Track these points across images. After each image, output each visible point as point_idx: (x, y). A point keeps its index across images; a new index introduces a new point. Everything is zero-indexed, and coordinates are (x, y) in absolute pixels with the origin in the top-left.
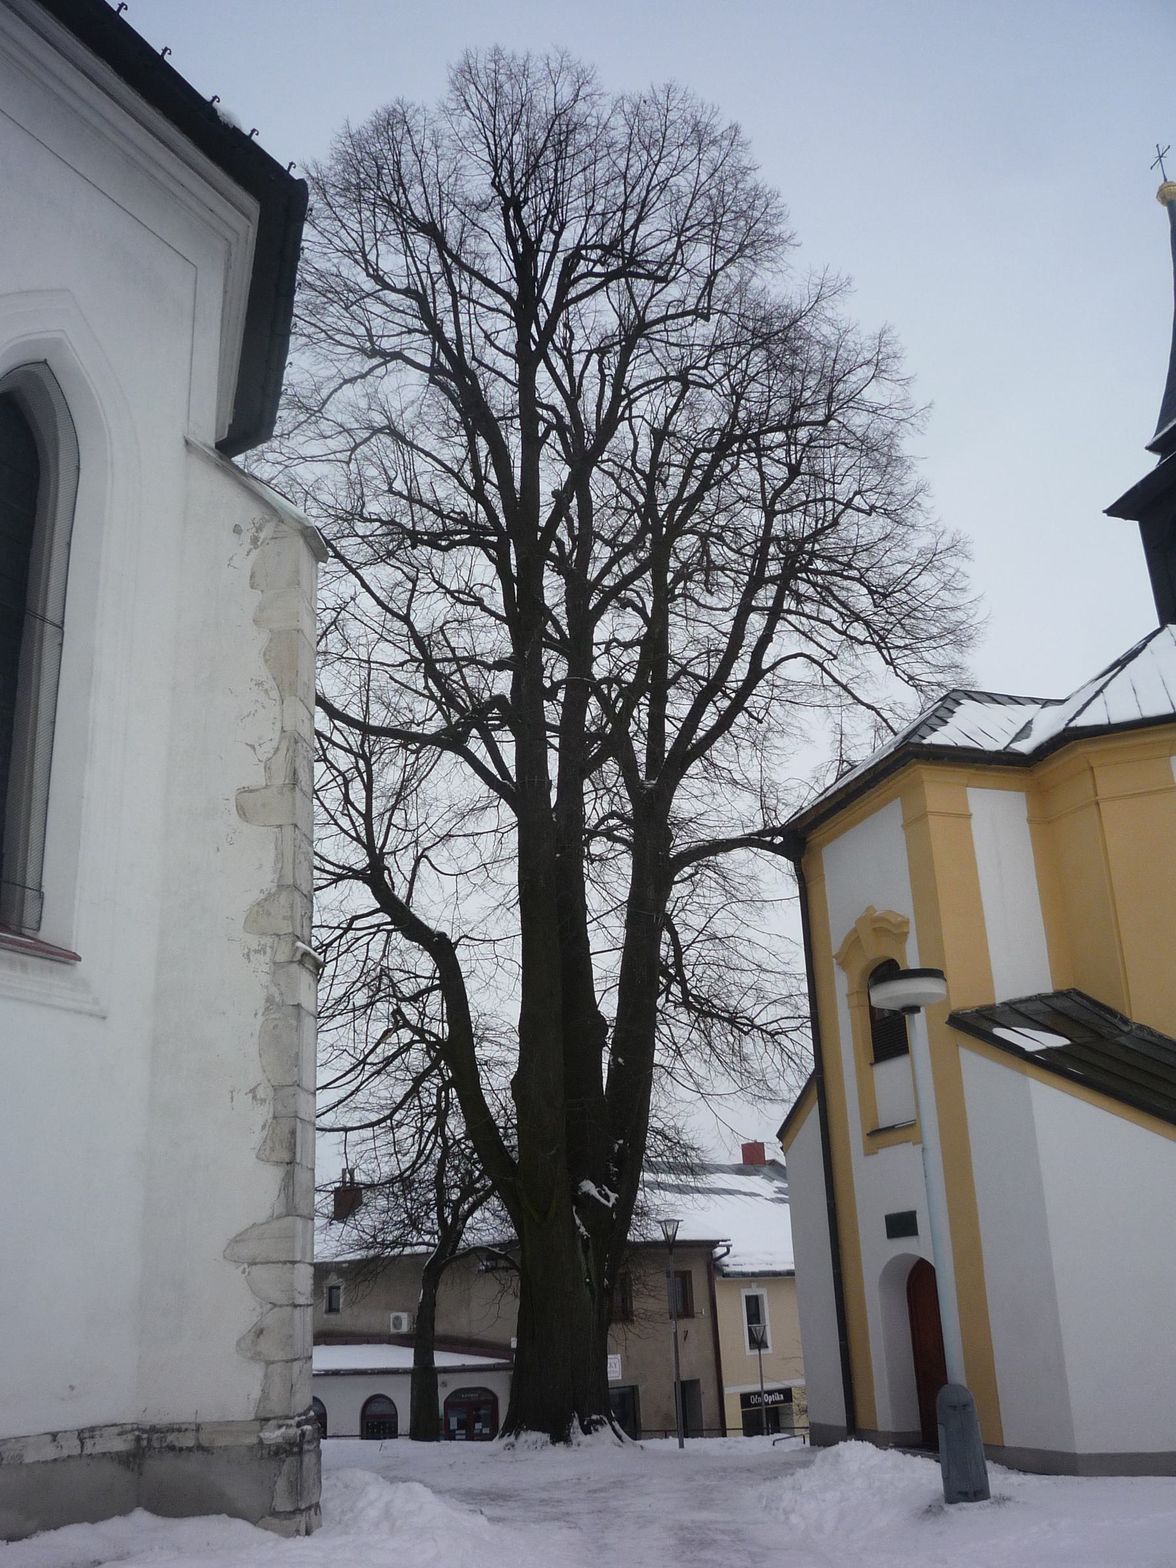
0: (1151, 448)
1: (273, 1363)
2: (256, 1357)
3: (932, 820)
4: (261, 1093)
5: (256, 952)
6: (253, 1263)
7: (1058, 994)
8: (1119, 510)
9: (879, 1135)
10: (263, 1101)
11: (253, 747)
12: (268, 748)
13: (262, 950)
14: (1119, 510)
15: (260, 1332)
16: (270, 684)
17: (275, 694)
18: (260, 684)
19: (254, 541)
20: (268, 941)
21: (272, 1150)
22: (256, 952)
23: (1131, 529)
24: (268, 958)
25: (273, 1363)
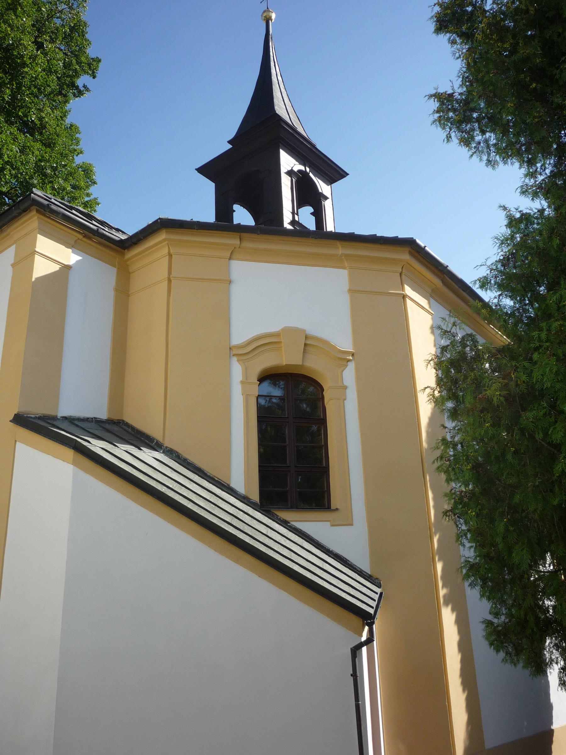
3: (37, 258)
7: (110, 421)
8: (205, 170)
14: (205, 170)
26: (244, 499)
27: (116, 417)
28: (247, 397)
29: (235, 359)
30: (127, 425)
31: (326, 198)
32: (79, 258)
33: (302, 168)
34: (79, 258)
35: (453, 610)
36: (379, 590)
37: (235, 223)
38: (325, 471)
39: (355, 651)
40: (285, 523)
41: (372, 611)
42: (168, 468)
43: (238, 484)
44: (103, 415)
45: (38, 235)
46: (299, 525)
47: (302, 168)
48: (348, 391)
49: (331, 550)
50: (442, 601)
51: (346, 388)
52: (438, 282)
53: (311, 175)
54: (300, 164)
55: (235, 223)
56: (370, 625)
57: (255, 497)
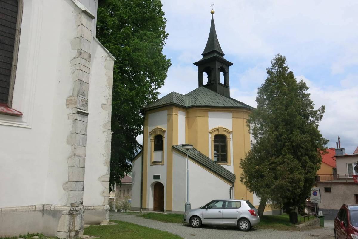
0: (202, 55)
1: (106, 197)
2: (103, 196)
4: (105, 155)
5: (105, 132)
6: (103, 182)
8: (196, 64)
9: (154, 163)
10: (105, 156)
11: (105, 97)
12: (107, 98)
13: (105, 132)
14: (196, 64)
15: (104, 192)
16: (108, 86)
17: (109, 88)
18: (106, 86)
19: (106, 60)
20: (106, 130)
21: (106, 164)
22: (105, 132)
23: (197, 68)
24: (106, 133)
25: (106, 197)
51: (230, 138)
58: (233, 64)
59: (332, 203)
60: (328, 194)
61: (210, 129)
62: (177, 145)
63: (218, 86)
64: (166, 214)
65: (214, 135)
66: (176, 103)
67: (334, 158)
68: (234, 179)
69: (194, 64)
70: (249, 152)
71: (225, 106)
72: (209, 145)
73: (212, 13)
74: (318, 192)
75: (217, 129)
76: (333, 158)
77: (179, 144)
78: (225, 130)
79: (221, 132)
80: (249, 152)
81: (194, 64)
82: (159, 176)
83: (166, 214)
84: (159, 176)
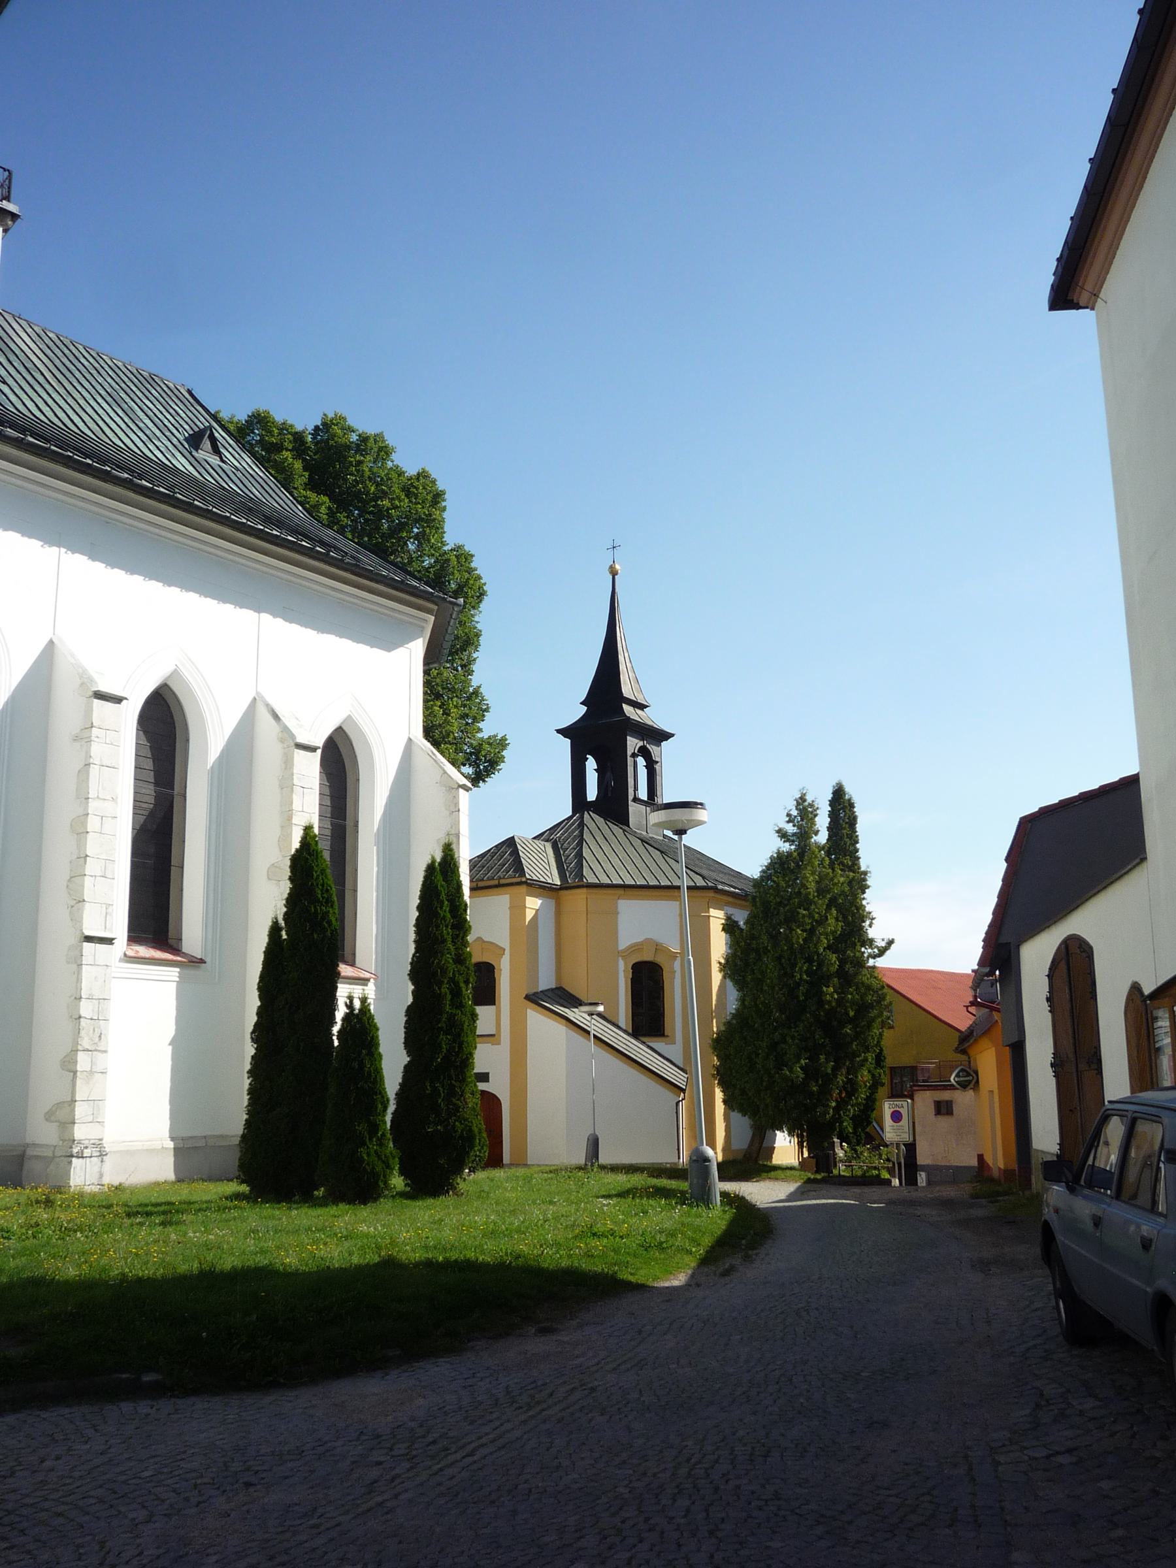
3: (527, 910)
7: (557, 988)
8: (563, 732)
14: (563, 732)
26: (625, 1031)
27: (558, 986)
28: (626, 978)
29: (620, 958)
30: (564, 989)
31: (657, 762)
32: (541, 901)
33: (641, 744)
34: (541, 901)
35: (790, 1134)
36: (686, 1076)
37: (588, 800)
38: (663, 1015)
39: (677, 1104)
40: (643, 1043)
41: (684, 1087)
42: (666, 1055)
43: (622, 1025)
44: (554, 987)
45: (528, 898)
46: (650, 1044)
47: (641, 744)
48: (676, 974)
49: (285, 909)
50: (507, 952)
52: (731, 899)
53: (648, 746)
54: (641, 740)
55: (588, 800)
56: (684, 1093)
57: (630, 1031)
58: (671, 735)
59: (954, 1146)
60: (944, 1122)
61: (624, 942)
62: (537, 993)
63: (633, 808)
64: (144, 482)
65: (632, 963)
66: (535, 878)
67: (970, 1009)
68: (422, 624)
69: (558, 731)
70: (482, 581)
71: (662, 884)
72: (620, 1000)
73: (614, 573)
74: (904, 1112)
75: (636, 948)
76: (967, 1007)
77: (540, 990)
78: (658, 948)
79: (647, 957)
80: (482, 581)
81: (558, 731)
82: (488, 1074)
83: (144, 482)
84: (488, 1074)
